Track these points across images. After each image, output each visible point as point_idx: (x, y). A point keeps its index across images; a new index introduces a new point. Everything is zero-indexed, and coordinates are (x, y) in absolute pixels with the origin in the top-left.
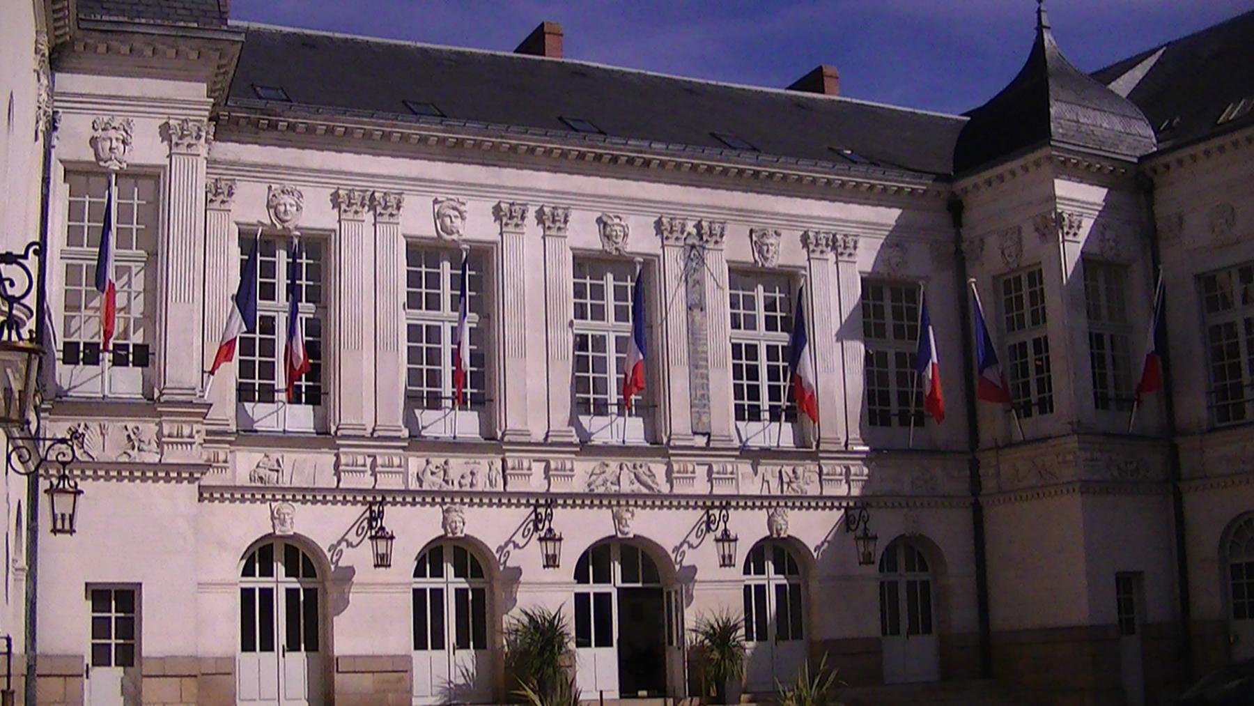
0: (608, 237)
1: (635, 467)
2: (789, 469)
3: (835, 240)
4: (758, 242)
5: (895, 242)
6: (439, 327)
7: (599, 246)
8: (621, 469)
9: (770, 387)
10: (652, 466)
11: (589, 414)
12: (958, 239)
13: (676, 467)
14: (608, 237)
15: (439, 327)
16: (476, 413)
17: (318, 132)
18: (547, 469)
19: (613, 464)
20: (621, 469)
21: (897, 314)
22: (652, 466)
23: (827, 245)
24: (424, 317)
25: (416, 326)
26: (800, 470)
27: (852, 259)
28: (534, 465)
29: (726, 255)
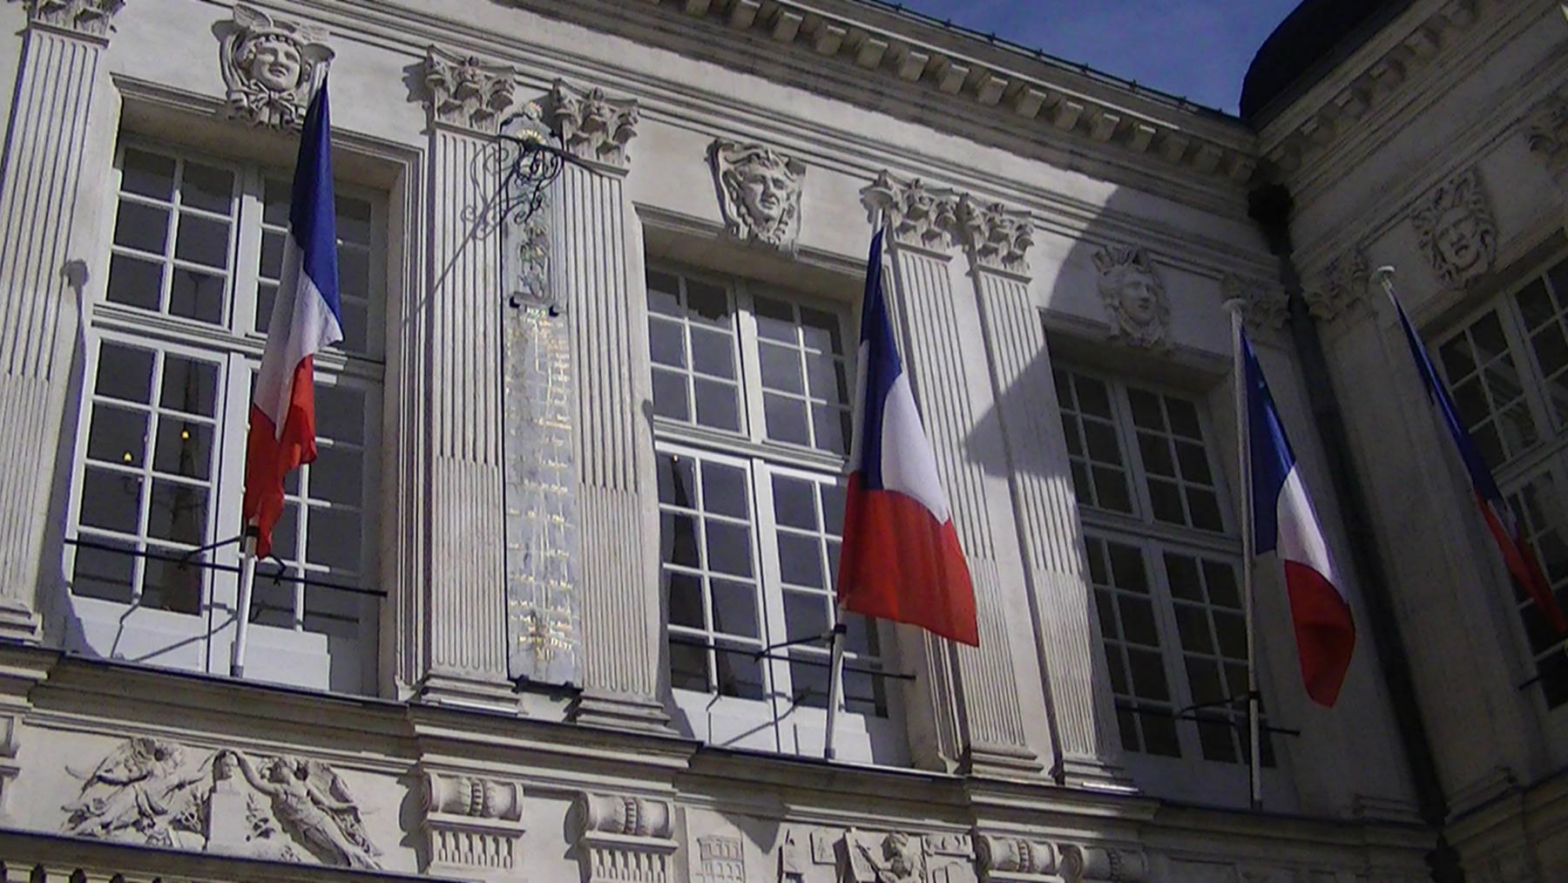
0: (247, 68)
1: (275, 775)
2: (873, 842)
3: (963, 211)
4: (737, 175)
5: (1102, 242)
6: (213, 368)
7: (217, 90)
8: (220, 773)
9: (87, 469)
10: (351, 782)
11: (708, 690)
12: (1290, 277)
13: (441, 790)
14: (247, 68)
15: (213, 368)
16: (323, 638)
17: (904, 72)
18: (577, 823)
19: (189, 759)
20: (220, 773)
21: (1153, 454)
22: (351, 782)
23: (942, 221)
24: (163, 336)
25: (192, 363)
26: (910, 848)
27: (1015, 269)
28: (528, 805)
29: (635, 188)
